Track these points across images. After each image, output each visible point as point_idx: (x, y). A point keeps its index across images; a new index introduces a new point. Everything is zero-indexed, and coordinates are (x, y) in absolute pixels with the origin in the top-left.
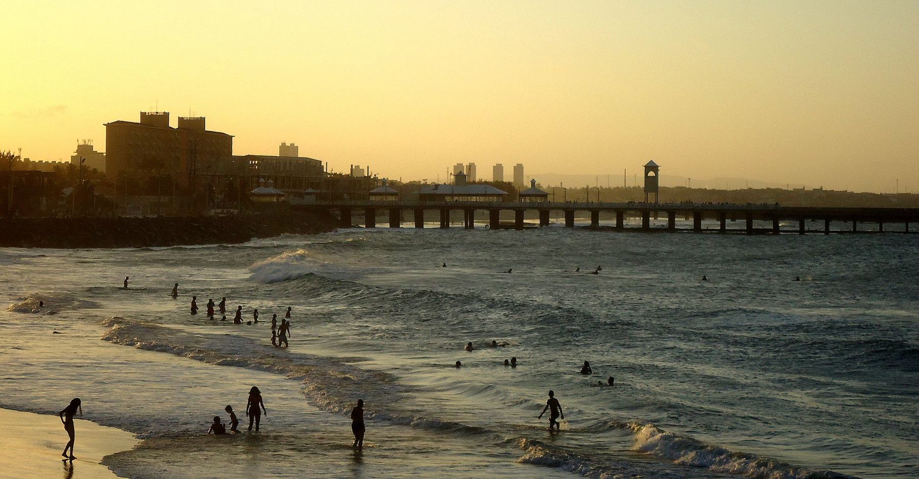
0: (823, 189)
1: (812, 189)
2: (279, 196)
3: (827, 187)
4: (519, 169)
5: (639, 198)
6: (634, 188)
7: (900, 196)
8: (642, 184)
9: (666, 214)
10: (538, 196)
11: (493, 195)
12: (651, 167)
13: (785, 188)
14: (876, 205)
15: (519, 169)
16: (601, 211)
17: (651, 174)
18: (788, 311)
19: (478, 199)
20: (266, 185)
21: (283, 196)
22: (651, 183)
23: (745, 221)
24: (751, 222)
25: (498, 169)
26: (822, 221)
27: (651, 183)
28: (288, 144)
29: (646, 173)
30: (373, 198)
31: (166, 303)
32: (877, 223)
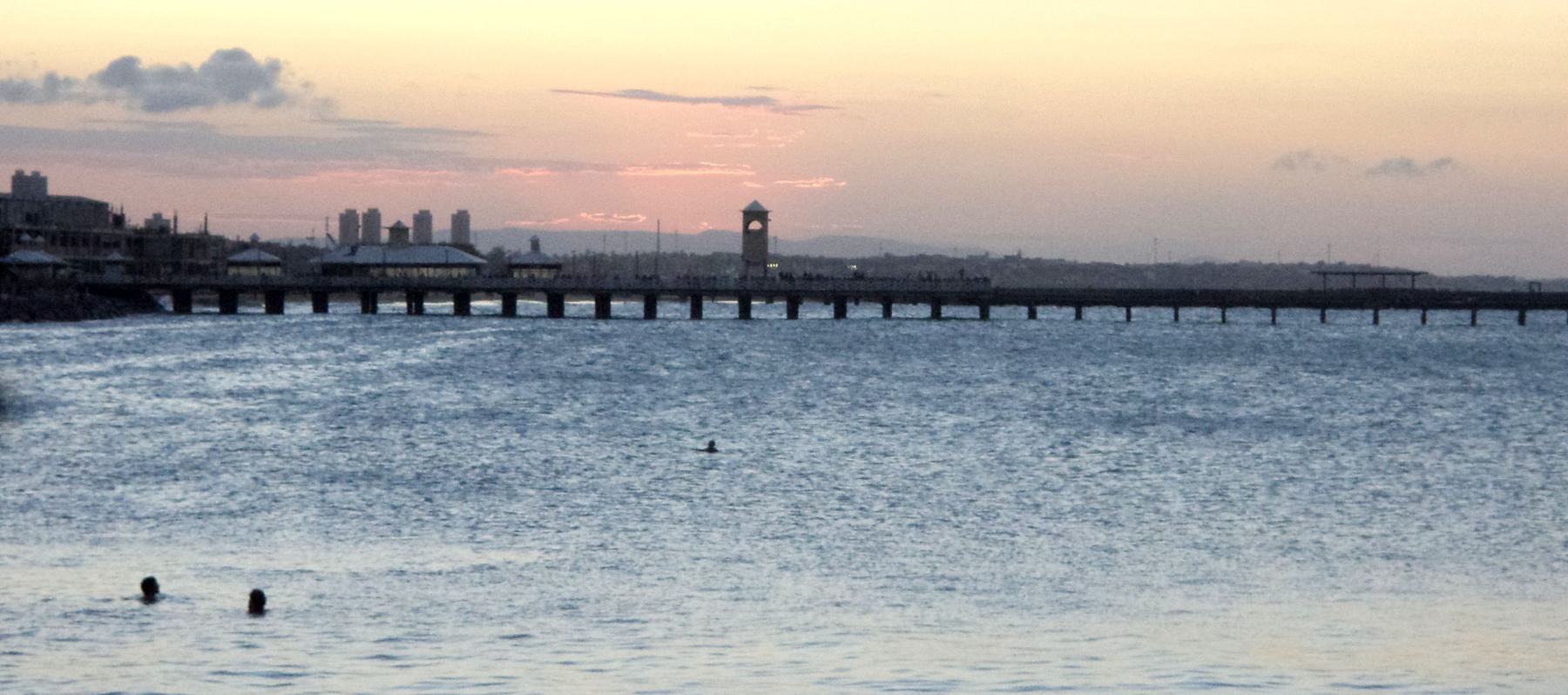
0: (1024, 257)
1: (1002, 257)
2: (57, 266)
3: (1031, 253)
4: (461, 220)
5: (733, 272)
6: (675, 255)
7: (1159, 268)
8: (737, 248)
9: (545, 296)
10: (543, 266)
11: (460, 265)
12: (755, 213)
13: (950, 255)
14: (1492, 289)
15: (461, 220)
16: (382, 292)
17: (755, 225)
18: (124, 362)
19: (430, 272)
20: (33, 246)
21: (64, 266)
22: (755, 241)
23: (736, 302)
24: (939, 309)
25: (423, 219)
26: (781, 303)
27: (755, 241)
28: (28, 173)
29: (746, 224)
30: (232, 271)
31: (438, 663)
32: (827, 303)
